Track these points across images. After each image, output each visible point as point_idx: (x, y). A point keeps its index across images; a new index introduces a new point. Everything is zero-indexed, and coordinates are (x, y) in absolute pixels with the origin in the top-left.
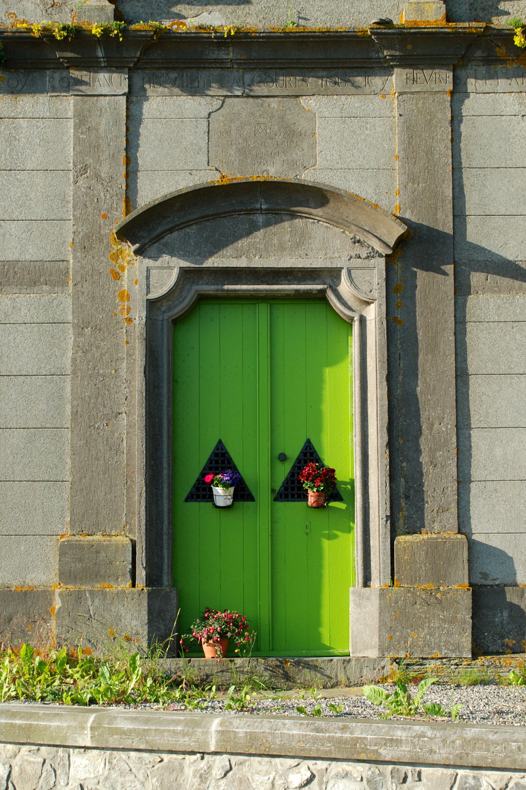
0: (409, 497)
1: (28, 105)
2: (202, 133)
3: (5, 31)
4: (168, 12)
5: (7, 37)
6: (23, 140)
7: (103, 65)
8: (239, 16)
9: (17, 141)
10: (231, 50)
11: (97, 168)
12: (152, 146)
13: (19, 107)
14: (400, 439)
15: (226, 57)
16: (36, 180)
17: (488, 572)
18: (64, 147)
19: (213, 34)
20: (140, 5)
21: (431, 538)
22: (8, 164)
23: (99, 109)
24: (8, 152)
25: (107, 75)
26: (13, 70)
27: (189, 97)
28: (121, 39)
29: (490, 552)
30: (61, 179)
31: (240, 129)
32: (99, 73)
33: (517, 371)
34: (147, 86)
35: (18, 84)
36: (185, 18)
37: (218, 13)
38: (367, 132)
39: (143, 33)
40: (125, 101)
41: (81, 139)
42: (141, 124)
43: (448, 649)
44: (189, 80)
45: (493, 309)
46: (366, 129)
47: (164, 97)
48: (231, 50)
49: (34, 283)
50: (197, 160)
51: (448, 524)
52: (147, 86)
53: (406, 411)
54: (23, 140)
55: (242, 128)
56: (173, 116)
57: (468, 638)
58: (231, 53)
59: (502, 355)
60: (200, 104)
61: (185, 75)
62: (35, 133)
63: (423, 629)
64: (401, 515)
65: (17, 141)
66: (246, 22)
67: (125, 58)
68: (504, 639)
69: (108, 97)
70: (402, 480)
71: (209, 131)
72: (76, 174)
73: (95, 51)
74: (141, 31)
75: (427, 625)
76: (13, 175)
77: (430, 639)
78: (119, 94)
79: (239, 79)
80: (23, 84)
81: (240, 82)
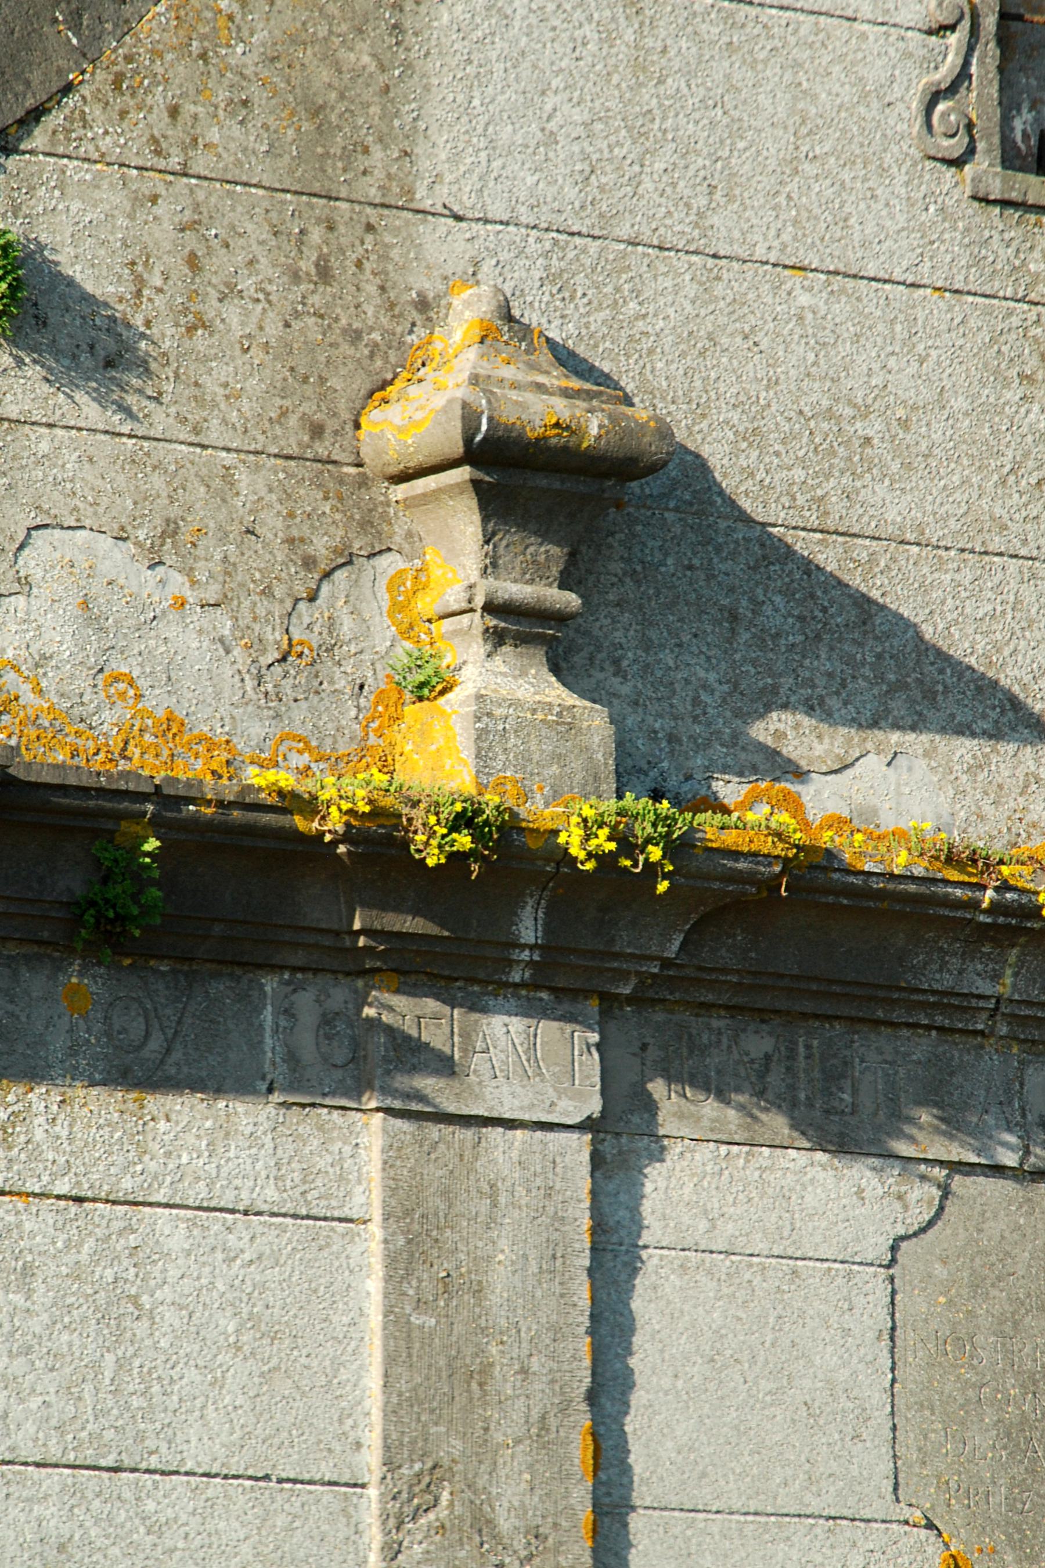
1: (190, 1138)
2: (871, 1335)
3: (193, 793)
4: (735, 736)
5: (196, 824)
6: (170, 1317)
7: (516, 977)
8: (1000, 787)
9: (145, 1323)
10: (1012, 959)
11: (480, 1483)
12: (680, 1384)
13: (154, 1146)
15: (984, 987)
16: (222, 1525)
18: (338, 1365)
19: (990, 894)
20: (626, 689)
22: (109, 1434)
23: (486, 1188)
24: (108, 1374)
25: (517, 1024)
26: (127, 962)
27: (820, 1156)
28: (663, 886)
30: (325, 1527)
31: (1008, 1327)
32: (484, 1010)
34: (657, 1088)
35: (147, 1035)
36: (800, 775)
37: (923, 763)
39: (742, 865)
40: (585, 1156)
41: (416, 1334)
42: (635, 1271)
44: (816, 1074)
47: (724, 1149)
48: (1012, 959)
50: (855, 1470)
52: (657, 1088)
54: (170, 1317)
55: (1016, 1324)
56: (761, 1246)
58: (1009, 972)
60: (860, 1193)
61: (801, 1050)
62: (221, 1287)
65: (145, 1323)
66: (1029, 818)
67: (617, 956)
69: (519, 1133)
71: (893, 1329)
72: (393, 1507)
73: (512, 915)
74: (735, 854)
76: (127, 1495)
78: (570, 1122)
79: (1008, 1091)
80: (170, 1033)
81: (1010, 1103)
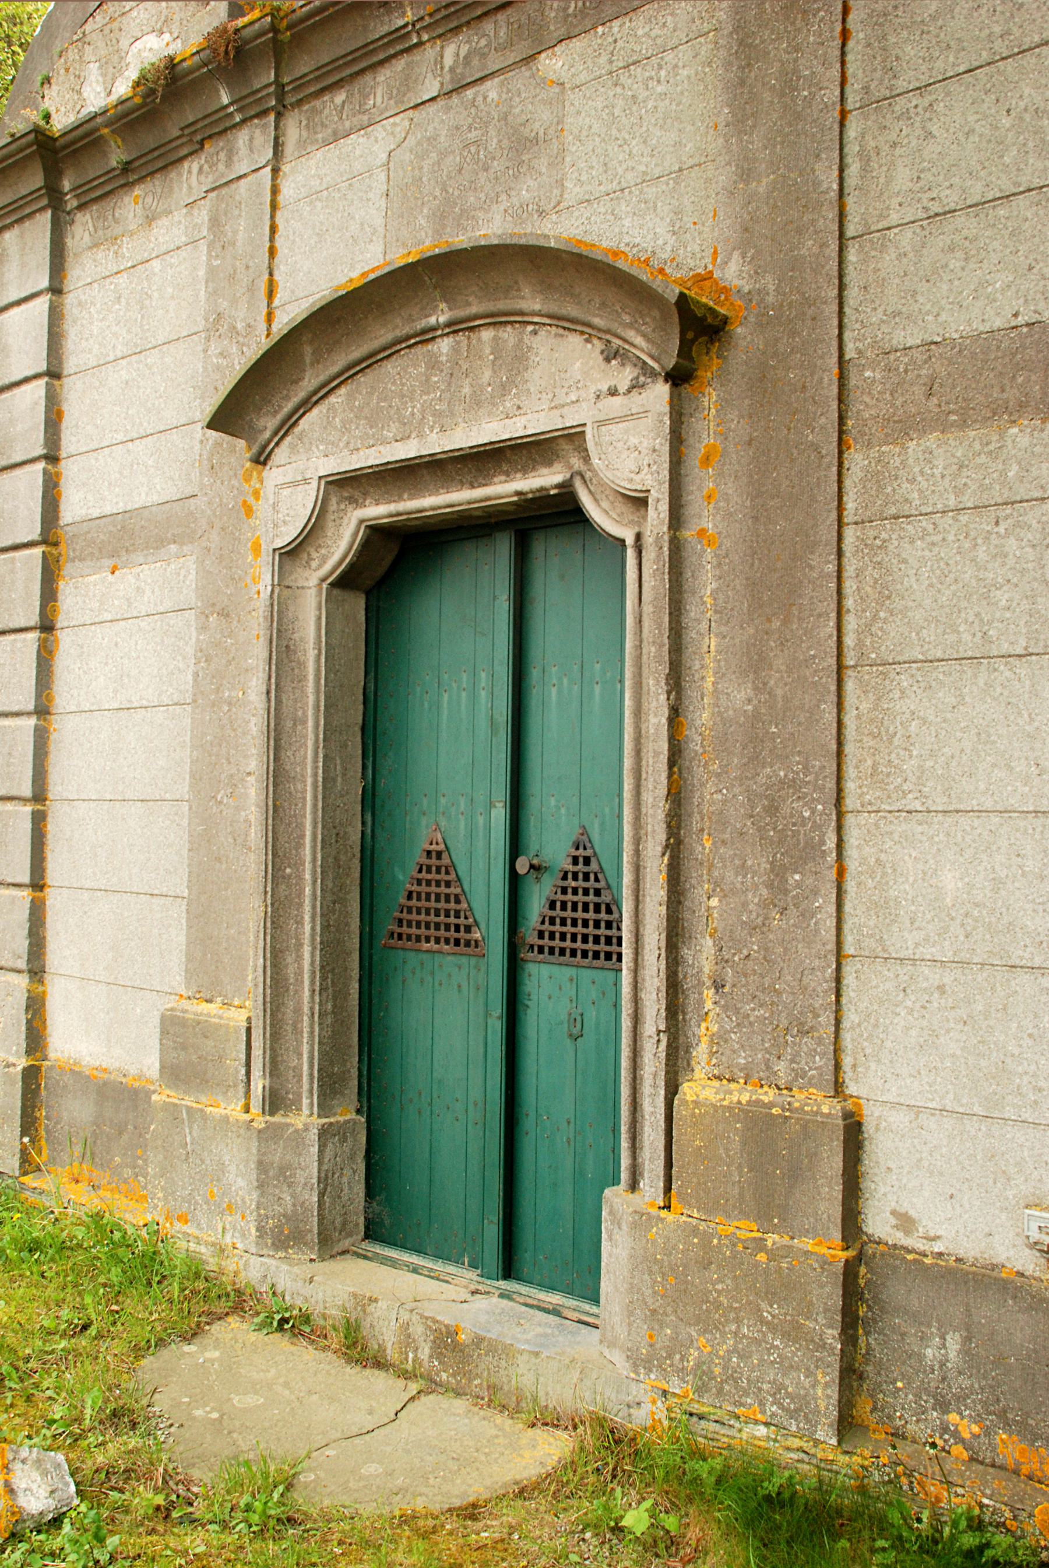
0: (723, 986)
14: (706, 837)
17: (912, 1213)
21: (758, 1103)
29: (921, 1159)
33: (1005, 648)
38: (659, 89)
43: (781, 1406)
45: (943, 477)
46: (659, 81)
49: (161, 542)
51: (811, 1069)
53: (720, 767)
57: (829, 1391)
59: (964, 604)
63: (723, 1334)
64: (703, 1030)
68: (948, 1412)
70: (710, 942)
75: (734, 1327)
77: (738, 1365)
